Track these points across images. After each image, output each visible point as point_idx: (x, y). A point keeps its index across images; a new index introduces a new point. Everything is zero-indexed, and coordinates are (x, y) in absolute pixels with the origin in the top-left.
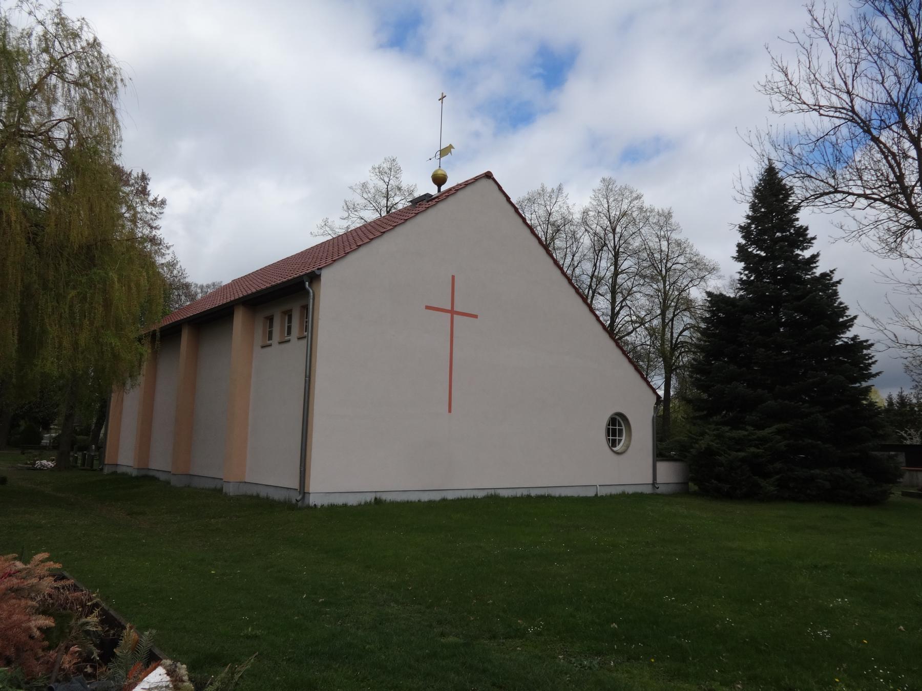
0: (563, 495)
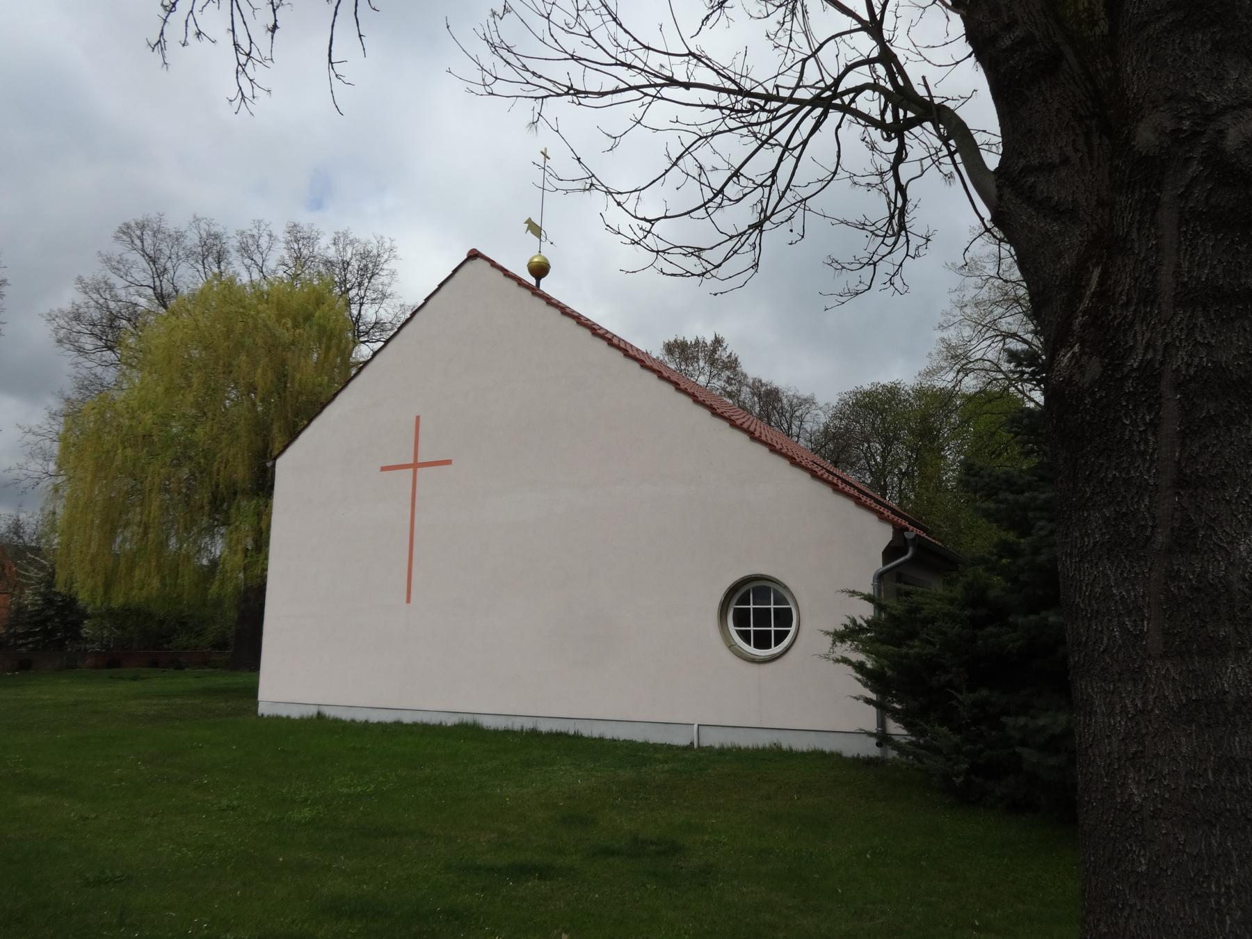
0: (608, 736)
